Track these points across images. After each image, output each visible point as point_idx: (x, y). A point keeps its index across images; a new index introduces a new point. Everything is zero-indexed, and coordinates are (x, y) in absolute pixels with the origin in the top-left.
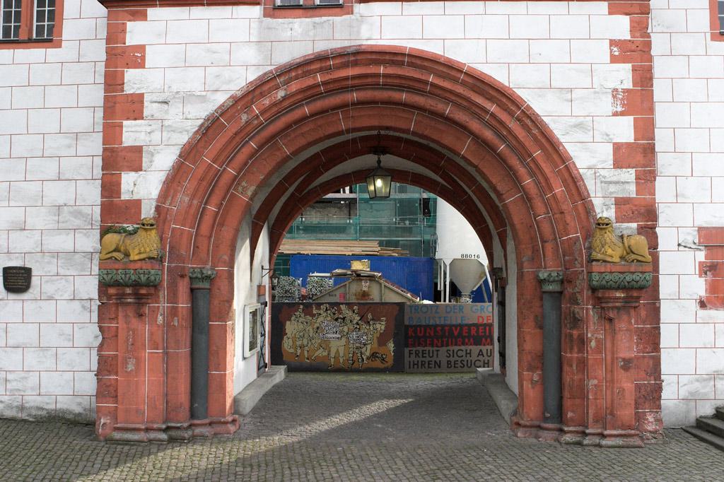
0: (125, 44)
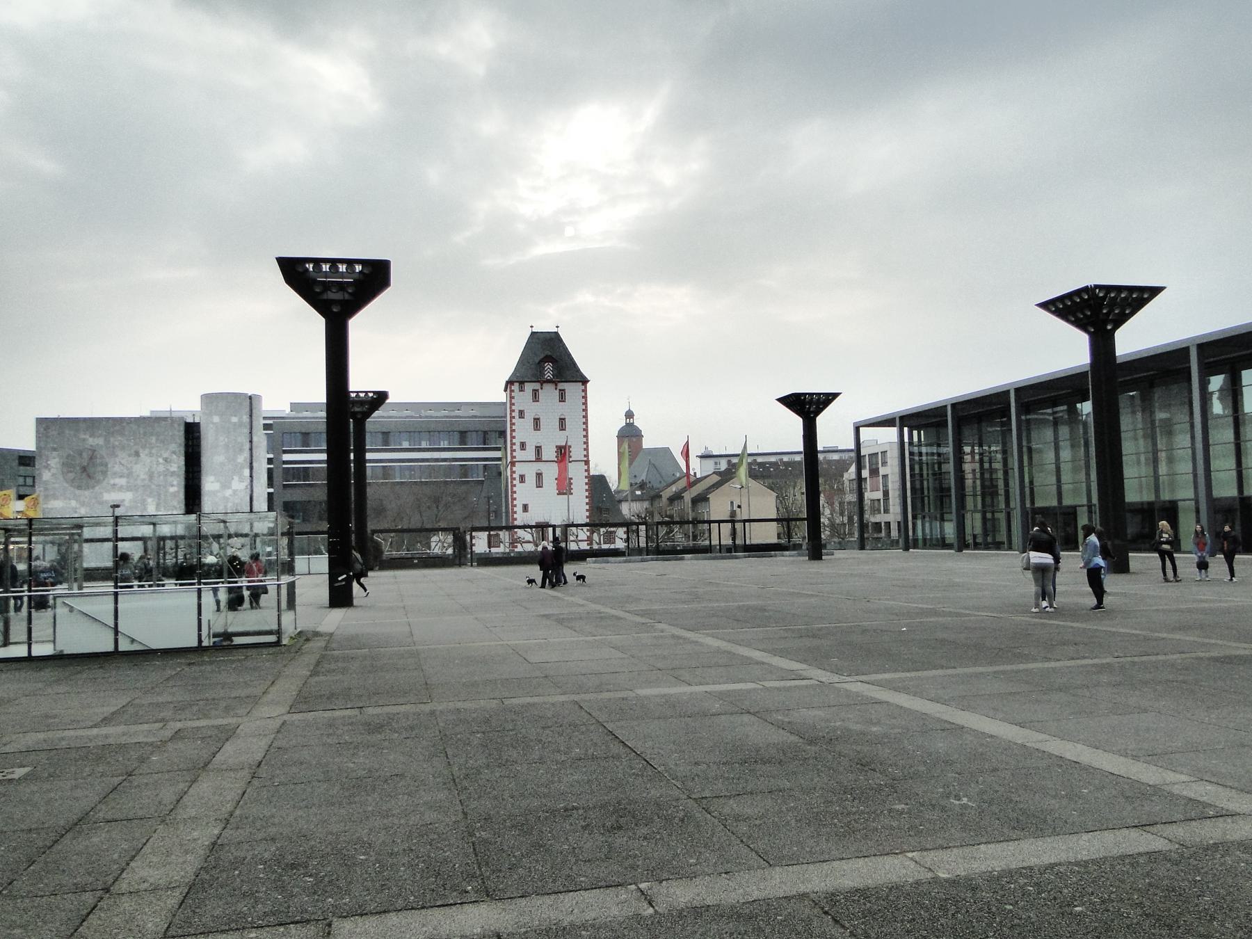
0: (879, 500)
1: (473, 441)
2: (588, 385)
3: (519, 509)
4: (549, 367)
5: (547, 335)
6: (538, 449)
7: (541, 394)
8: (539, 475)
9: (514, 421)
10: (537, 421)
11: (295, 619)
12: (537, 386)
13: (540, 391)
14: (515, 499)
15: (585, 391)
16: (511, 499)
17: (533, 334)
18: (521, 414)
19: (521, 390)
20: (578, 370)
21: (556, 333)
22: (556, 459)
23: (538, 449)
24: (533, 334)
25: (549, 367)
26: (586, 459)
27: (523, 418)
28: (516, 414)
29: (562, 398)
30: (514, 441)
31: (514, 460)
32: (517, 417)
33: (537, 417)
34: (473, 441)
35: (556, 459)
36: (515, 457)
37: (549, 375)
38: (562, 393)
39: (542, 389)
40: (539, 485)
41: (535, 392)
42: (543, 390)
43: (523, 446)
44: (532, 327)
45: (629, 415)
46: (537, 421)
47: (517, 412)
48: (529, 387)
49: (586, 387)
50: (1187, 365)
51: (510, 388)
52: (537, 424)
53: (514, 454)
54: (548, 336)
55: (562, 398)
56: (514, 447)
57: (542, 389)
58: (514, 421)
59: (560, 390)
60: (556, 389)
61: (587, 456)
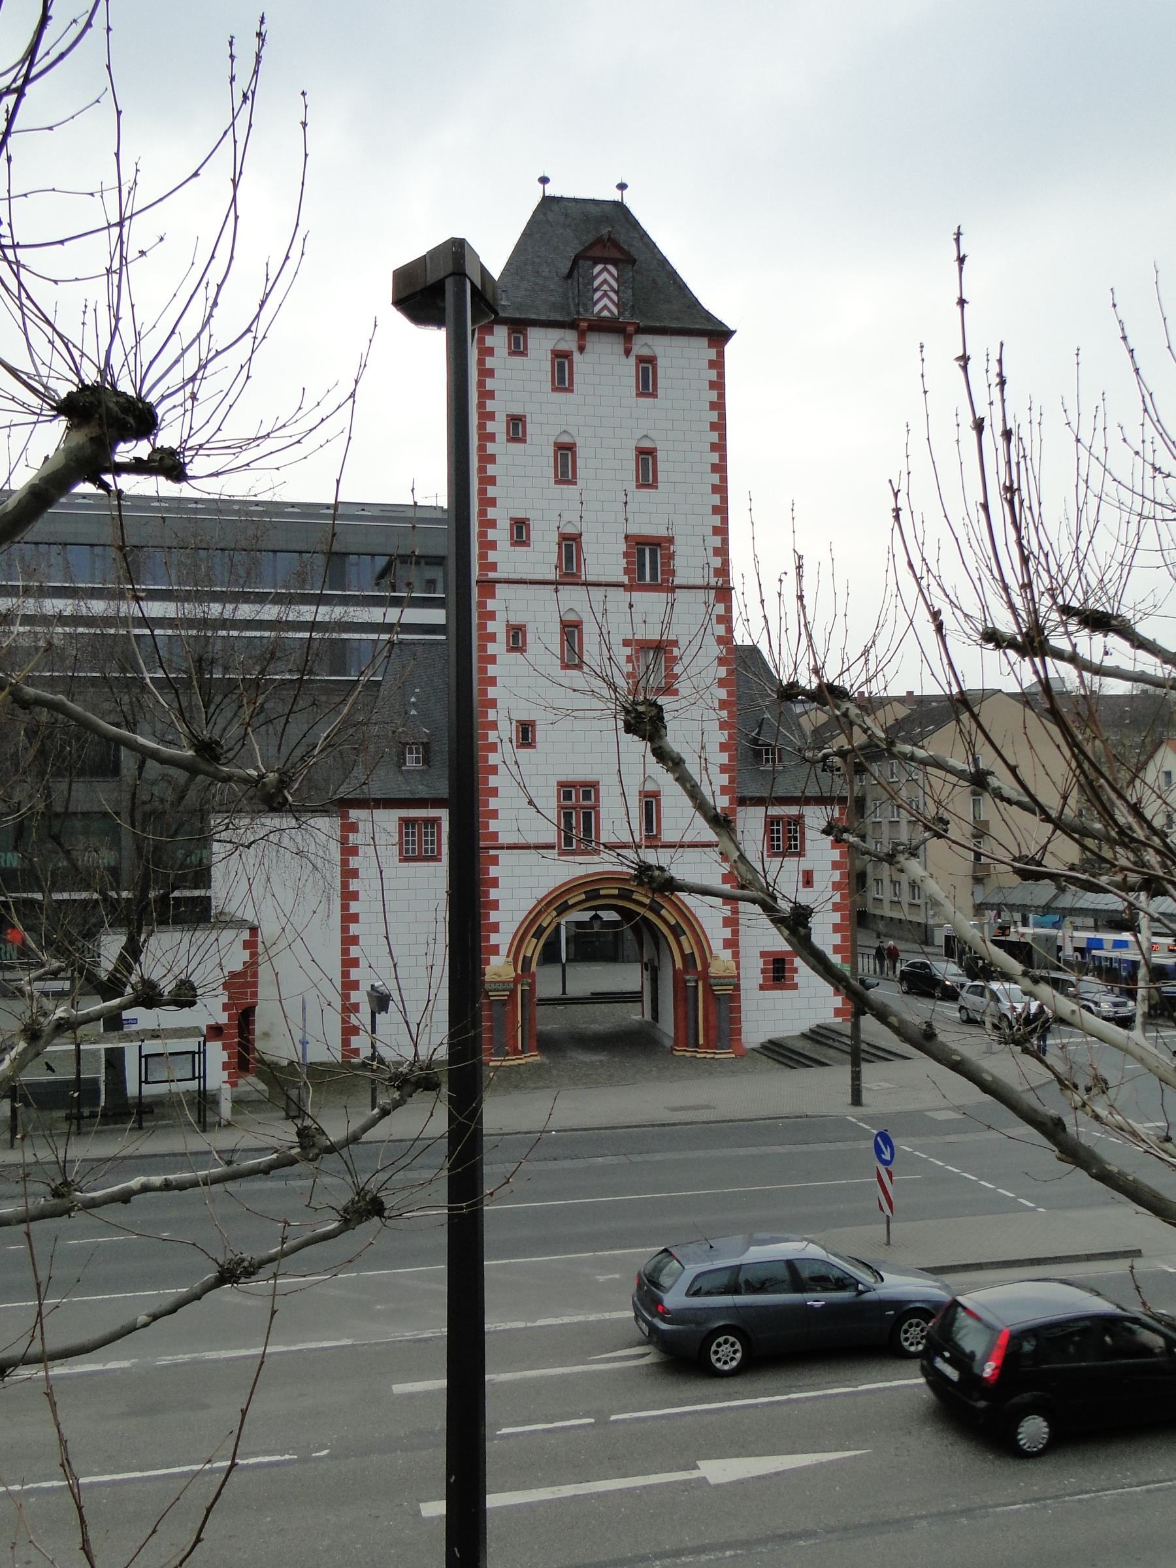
1: (361, 581)
2: (730, 348)
3: (501, 534)
4: (605, 276)
5: (591, 208)
6: (570, 545)
8: (571, 630)
9: (491, 448)
10: (565, 451)
11: (131, 1329)
12: (567, 340)
13: (577, 356)
14: (491, 395)
15: (718, 364)
16: (480, 616)
17: (548, 202)
18: (517, 426)
19: (518, 350)
20: (694, 304)
21: (620, 206)
22: (625, 579)
23: (570, 545)
24: (548, 202)
25: (605, 276)
27: (523, 440)
28: (498, 427)
29: (647, 386)
30: (492, 513)
31: (492, 575)
32: (501, 437)
33: (565, 439)
34: (361, 581)
35: (625, 579)
36: (493, 567)
37: (605, 305)
38: (645, 371)
39: (581, 349)
40: (572, 658)
41: (561, 359)
42: (588, 356)
43: (520, 530)
44: (544, 180)
45: (959, 227)
46: (565, 451)
47: (501, 418)
48: (542, 342)
49: (721, 355)
50: (743, 1291)
51: (481, 341)
52: (565, 466)
53: (492, 556)
54: (596, 210)
55: (647, 386)
56: (492, 534)
57: (581, 349)
58: (491, 448)
59: (641, 360)
60: (627, 352)
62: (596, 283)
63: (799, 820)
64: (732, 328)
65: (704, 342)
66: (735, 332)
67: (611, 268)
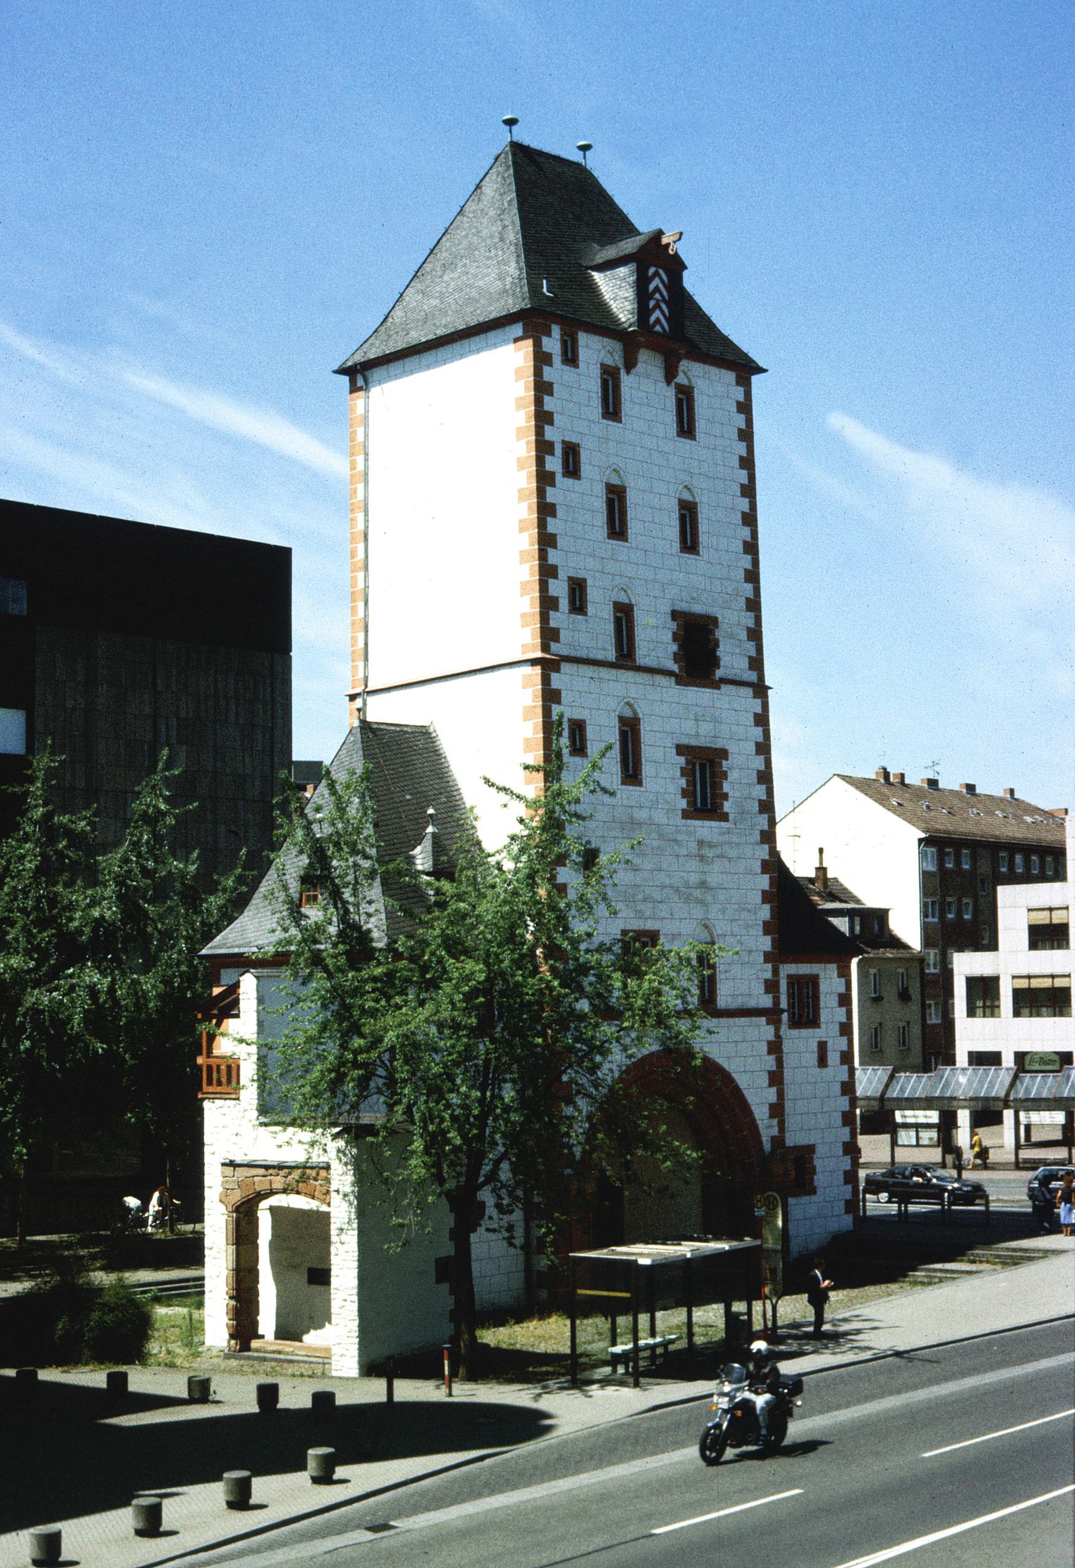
6: (624, 616)
7: (627, 382)
13: (623, 372)
23: (624, 616)
26: (752, 677)
32: (564, 604)
35: (675, 668)
61: (756, 663)
62: (652, 287)
63: (813, 981)
64: (762, 364)
65: (730, 376)
66: (765, 371)
67: (661, 272)
